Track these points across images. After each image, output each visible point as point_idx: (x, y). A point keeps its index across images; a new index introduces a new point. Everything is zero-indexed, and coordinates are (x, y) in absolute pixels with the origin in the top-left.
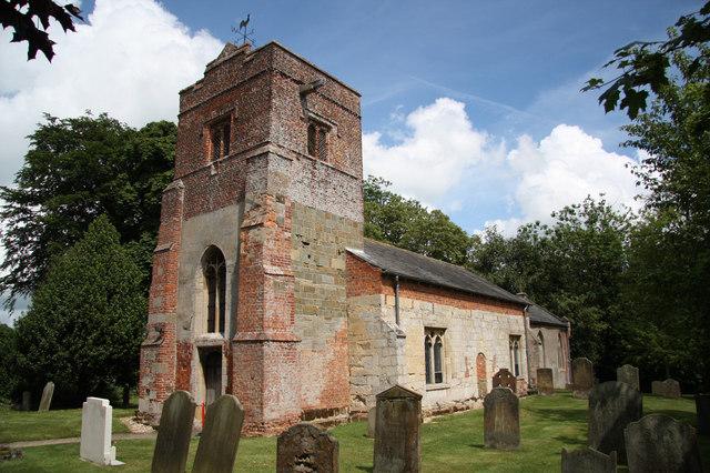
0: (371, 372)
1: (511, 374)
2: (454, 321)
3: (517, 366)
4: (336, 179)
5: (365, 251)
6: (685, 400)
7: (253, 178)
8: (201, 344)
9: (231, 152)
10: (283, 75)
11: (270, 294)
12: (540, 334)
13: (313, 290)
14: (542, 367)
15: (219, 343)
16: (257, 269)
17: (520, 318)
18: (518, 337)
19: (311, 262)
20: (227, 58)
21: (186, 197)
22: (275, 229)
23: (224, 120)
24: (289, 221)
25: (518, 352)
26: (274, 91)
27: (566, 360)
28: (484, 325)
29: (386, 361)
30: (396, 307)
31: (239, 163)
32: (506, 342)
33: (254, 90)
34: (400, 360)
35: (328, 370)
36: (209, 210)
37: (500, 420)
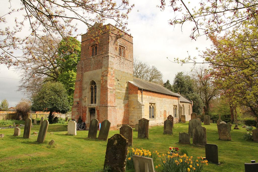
7: (104, 63)
9: (98, 54)
11: (109, 94)
12: (183, 105)
13: (120, 93)
15: (94, 107)
17: (177, 101)
18: (176, 106)
19: (119, 85)
30: (142, 97)
31: (100, 58)
33: (104, 37)
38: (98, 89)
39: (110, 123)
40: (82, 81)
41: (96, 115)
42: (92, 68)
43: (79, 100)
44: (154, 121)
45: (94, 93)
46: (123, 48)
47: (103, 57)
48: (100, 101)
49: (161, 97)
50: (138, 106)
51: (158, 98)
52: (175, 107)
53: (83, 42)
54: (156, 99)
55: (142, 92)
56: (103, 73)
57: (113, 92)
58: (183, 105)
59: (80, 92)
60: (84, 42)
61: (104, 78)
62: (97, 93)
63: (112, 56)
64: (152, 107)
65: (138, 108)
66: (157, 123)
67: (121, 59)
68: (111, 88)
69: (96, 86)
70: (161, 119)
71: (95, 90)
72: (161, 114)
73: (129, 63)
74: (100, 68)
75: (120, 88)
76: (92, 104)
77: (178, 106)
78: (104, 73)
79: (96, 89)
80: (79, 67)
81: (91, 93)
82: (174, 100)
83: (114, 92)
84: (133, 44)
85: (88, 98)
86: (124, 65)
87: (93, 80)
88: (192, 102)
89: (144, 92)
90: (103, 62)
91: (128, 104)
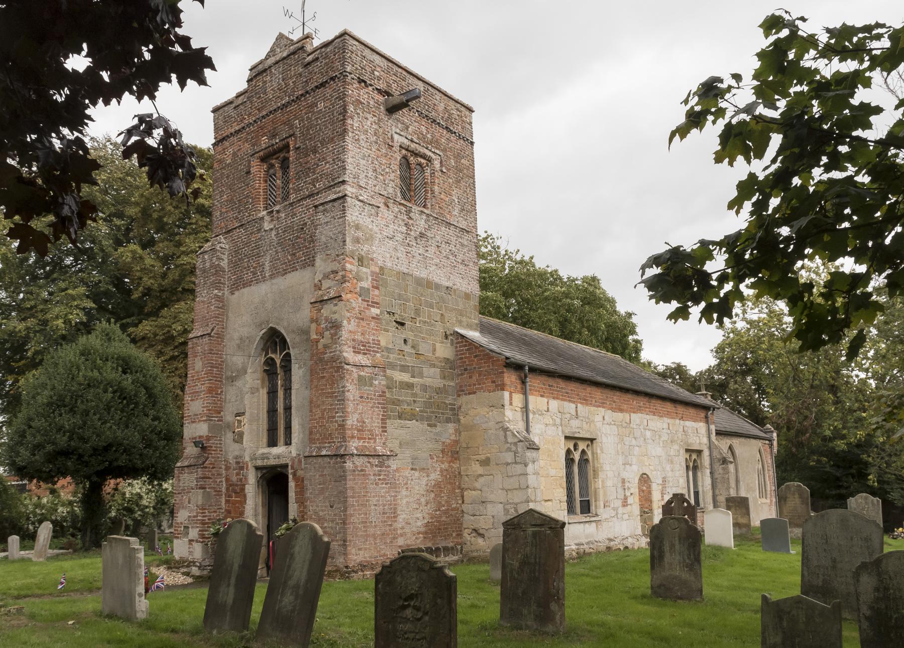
0: (492, 497)
1: (688, 502)
2: (606, 429)
3: (696, 494)
4: (440, 233)
5: (481, 332)
6: (739, 417)
7: (324, 234)
8: (259, 463)
9: (292, 197)
10: (361, 81)
11: (352, 391)
12: (731, 448)
13: (410, 386)
14: (733, 493)
15: (282, 461)
16: (334, 359)
17: (701, 426)
18: (699, 452)
19: (408, 349)
20: (278, 58)
21: (230, 262)
22: (356, 303)
23: (280, 150)
24: (376, 292)
25: (699, 474)
26: (351, 108)
27: (771, 486)
28: (648, 434)
29: (512, 483)
30: (526, 409)
31: (302, 213)
32: (681, 458)
33: (321, 106)
34: (532, 480)
35: (433, 495)
36: (264, 279)
37: (674, 560)
38: (298, 373)
39: (674, 495)
40: (220, 336)
41: (290, 505)
42: (267, 267)
43: (209, 431)
44: (591, 529)
45: (281, 394)
46: (420, 164)
47: (316, 207)
48: (307, 432)
49: (621, 411)
50: (509, 450)
51: (609, 415)
52: (694, 456)
53: (223, 139)
54: (598, 418)
55: (524, 383)
56: (318, 287)
57: (376, 382)
58: (731, 448)
59: (210, 391)
60: (226, 144)
61: (326, 311)
62: (293, 392)
63: (361, 198)
64: (577, 456)
65: (508, 464)
66: (610, 540)
67: (412, 215)
68: (361, 359)
69: (287, 359)
70: (626, 517)
71: (285, 380)
72: (628, 494)
73: (453, 239)
74: (304, 267)
75: (410, 361)
76: (275, 451)
77: (706, 453)
78: (326, 284)
79: (287, 368)
80: (208, 265)
81: (268, 393)
82: (689, 424)
83: (380, 382)
84: (472, 143)
85: (251, 421)
86: (432, 249)
87: (271, 327)
88: (775, 435)
89: (533, 381)
90: (320, 228)
91: (457, 442)
